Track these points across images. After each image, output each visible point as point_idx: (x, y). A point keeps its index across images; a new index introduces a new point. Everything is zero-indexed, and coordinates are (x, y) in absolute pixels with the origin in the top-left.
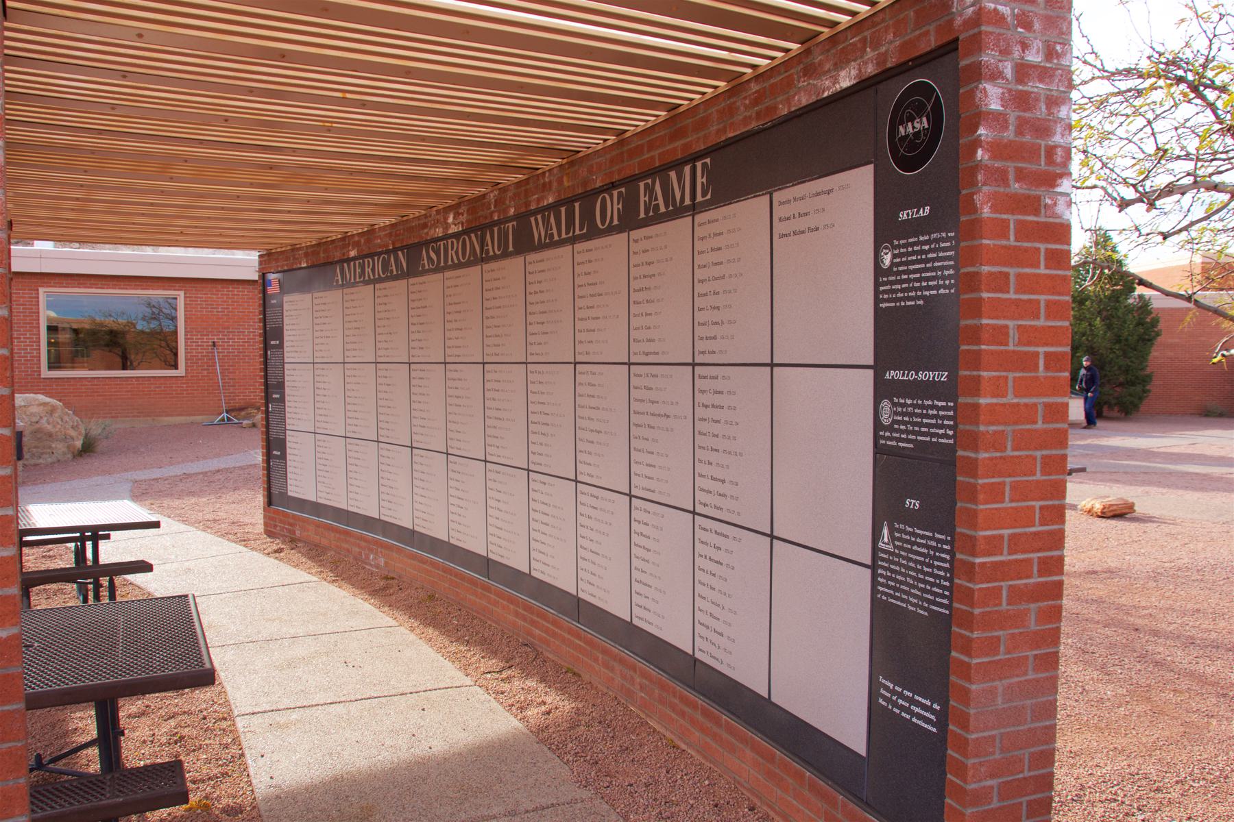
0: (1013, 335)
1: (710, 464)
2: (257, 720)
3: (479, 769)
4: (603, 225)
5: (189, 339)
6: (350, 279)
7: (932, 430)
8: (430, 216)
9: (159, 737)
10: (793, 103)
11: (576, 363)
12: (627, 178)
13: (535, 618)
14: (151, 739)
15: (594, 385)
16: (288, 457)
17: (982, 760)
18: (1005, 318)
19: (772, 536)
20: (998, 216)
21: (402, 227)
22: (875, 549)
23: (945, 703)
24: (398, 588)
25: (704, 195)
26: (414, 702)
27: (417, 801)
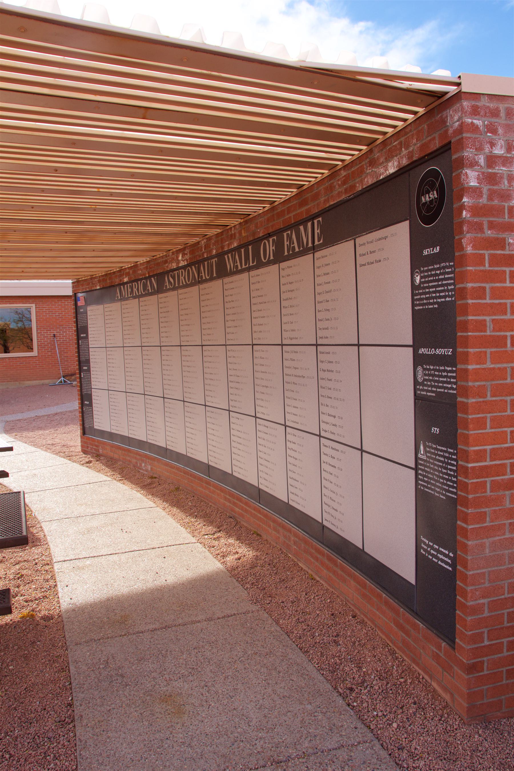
0: (489, 325)
1: (327, 406)
2: (65, 565)
3: (193, 593)
4: (265, 260)
5: (39, 333)
6: (125, 296)
7: (445, 385)
8: (169, 256)
9: (9, 575)
10: (364, 183)
11: (253, 345)
12: (277, 230)
13: (235, 501)
14: (5, 576)
15: (263, 358)
16: (94, 405)
17: (477, 587)
18: (483, 315)
19: (362, 450)
20: (477, 252)
21: (153, 263)
22: (417, 458)
23: (455, 553)
24: (158, 484)
25: (319, 241)
26: (159, 553)
27: (154, 612)
